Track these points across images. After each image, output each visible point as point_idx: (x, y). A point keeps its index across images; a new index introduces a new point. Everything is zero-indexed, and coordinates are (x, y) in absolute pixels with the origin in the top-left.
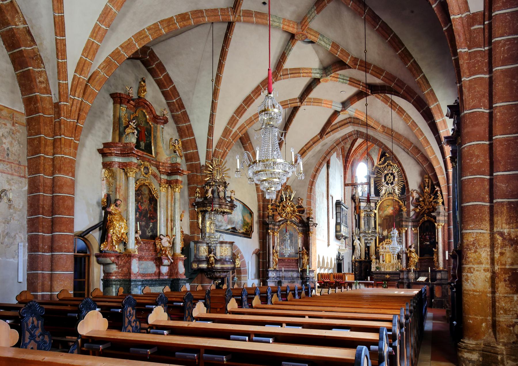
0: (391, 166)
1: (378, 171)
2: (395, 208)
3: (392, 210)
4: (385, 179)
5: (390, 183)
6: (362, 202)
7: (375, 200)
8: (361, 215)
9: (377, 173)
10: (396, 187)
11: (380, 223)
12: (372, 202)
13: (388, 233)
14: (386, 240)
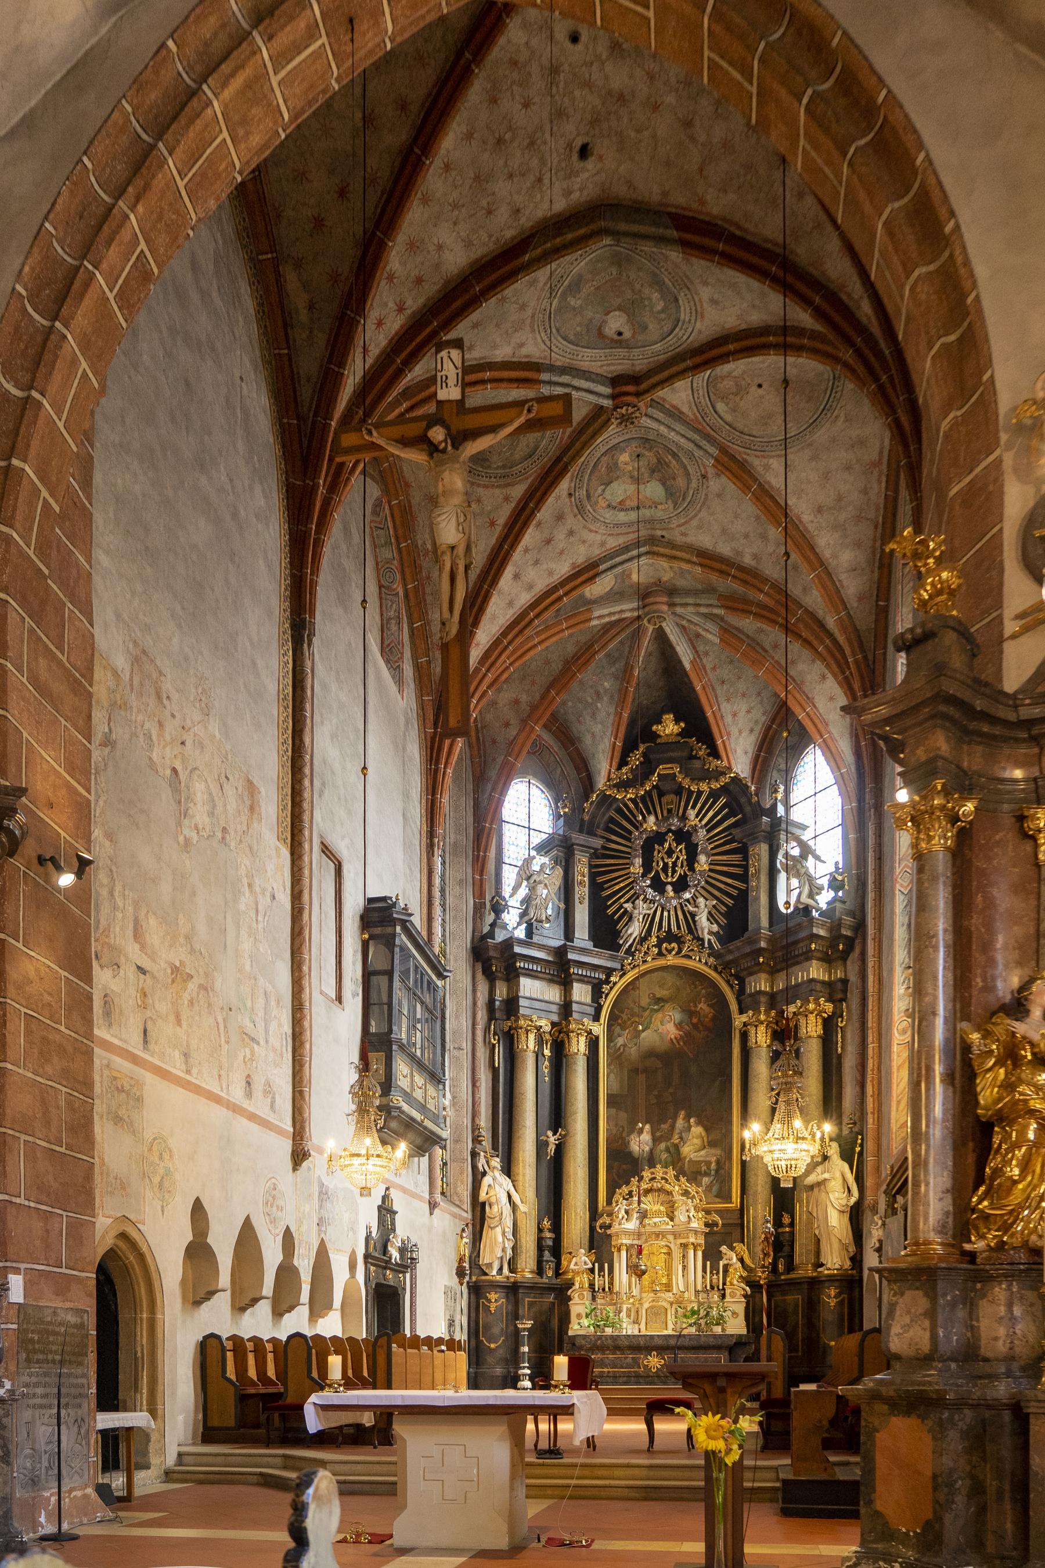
0: (679, 791)
1: (612, 820)
2: (690, 1013)
3: (679, 1026)
4: (647, 866)
5: (671, 883)
6: (531, 974)
7: (595, 967)
8: (522, 1045)
9: (608, 830)
10: (701, 901)
11: (616, 1089)
12: (582, 980)
13: (656, 1140)
14: (647, 1174)
